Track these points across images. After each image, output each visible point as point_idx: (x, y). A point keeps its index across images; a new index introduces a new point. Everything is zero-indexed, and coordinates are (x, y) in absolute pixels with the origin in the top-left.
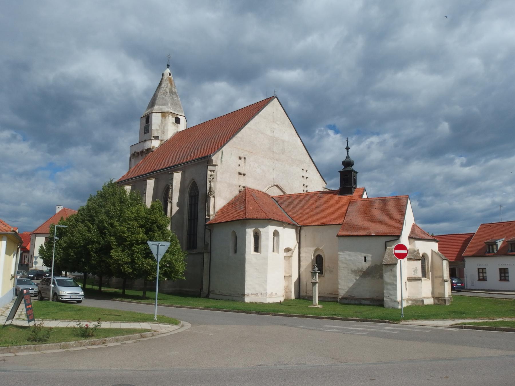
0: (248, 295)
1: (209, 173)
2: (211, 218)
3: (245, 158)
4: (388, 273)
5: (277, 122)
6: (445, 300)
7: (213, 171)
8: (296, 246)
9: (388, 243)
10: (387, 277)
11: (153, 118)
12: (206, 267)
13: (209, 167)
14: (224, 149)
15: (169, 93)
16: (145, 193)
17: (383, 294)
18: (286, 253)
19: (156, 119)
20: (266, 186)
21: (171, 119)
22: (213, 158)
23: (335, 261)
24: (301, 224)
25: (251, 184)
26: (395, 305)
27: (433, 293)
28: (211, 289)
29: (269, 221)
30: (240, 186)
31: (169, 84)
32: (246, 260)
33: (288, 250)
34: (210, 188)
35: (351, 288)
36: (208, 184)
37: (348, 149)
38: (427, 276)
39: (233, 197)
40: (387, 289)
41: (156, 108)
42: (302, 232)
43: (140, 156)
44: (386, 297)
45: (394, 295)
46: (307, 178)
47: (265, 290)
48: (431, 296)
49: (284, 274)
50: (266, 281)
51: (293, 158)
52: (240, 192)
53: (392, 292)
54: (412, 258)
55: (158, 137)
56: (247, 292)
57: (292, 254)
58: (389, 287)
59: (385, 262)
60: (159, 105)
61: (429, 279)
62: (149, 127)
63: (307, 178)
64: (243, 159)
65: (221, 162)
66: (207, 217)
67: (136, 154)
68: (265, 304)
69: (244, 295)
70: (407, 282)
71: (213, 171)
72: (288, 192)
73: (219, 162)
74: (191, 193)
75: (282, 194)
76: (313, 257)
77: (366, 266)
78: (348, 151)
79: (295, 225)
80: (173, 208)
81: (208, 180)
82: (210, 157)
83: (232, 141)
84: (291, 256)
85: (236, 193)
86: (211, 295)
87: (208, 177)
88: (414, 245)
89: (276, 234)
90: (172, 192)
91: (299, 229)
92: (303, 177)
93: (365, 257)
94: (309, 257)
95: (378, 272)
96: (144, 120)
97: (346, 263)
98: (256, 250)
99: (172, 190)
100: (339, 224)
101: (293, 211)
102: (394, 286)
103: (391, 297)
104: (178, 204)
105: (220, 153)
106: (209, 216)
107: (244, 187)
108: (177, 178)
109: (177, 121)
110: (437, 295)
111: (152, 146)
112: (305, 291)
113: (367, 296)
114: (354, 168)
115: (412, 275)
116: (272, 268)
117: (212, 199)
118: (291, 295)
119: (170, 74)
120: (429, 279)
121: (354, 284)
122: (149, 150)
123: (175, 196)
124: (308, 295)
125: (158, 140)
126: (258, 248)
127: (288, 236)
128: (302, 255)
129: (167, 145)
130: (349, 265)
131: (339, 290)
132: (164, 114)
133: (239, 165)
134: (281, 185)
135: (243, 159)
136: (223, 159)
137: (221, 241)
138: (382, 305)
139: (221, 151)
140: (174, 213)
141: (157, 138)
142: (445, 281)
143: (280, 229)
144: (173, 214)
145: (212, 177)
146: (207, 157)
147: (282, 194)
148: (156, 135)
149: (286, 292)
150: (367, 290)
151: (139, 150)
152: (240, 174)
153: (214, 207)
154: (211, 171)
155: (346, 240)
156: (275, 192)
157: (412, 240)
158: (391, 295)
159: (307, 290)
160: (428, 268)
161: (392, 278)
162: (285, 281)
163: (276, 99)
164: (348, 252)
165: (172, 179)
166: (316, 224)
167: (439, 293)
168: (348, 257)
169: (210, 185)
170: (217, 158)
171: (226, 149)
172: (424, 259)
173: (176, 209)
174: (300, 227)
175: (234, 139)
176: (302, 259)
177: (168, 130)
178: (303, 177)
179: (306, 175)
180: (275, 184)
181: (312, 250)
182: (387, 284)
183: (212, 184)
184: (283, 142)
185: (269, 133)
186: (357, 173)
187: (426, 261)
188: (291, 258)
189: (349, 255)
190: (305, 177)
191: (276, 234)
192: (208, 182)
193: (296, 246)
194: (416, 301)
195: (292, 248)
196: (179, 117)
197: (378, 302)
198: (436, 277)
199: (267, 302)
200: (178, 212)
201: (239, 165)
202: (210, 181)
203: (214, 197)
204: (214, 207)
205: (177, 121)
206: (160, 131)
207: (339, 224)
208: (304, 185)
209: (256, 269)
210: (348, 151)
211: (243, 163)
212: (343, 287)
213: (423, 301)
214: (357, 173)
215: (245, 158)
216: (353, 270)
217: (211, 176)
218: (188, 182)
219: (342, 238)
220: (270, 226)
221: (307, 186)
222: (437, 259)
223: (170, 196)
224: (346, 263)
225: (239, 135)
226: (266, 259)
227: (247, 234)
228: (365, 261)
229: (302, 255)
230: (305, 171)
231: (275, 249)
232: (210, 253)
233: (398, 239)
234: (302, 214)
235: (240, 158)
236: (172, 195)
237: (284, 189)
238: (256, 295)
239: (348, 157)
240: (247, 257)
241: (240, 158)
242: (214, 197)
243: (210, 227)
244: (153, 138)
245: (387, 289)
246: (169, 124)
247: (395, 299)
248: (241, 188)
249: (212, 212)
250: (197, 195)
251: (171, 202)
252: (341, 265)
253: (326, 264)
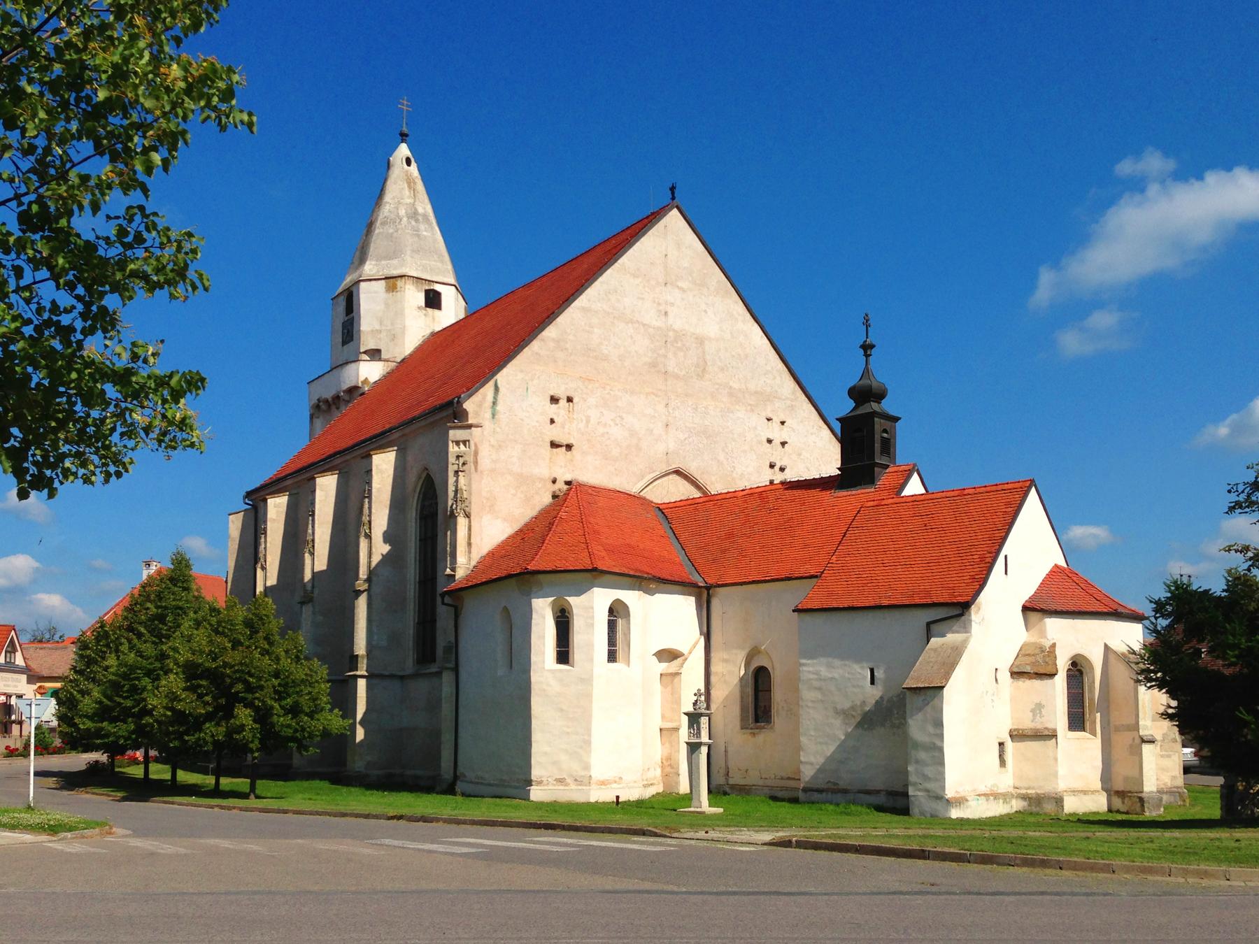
0: (540, 783)
1: (453, 449)
2: (460, 573)
3: (570, 400)
4: (920, 716)
5: (680, 284)
6: (1141, 800)
7: (464, 442)
8: (696, 643)
9: (934, 627)
10: (916, 727)
11: (362, 296)
12: (447, 709)
13: (451, 432)
14: (503, 377)
15: (405, 219)
16: (313, 515)
17: (906, 773)
18: (664, 665)
19: (371, 299)
20: (643, 477)
21: (416, 297)
22: (468, 405)
23: (794, 683)
24: (711, 581)
25: (590, 470)
26: (938, 807)
27: (1106, 777)
28: (461, 769)
29: (594, 575)
30: (554, 481)
31: (407, 192)
32: (534, 686)
33: (668, 655)
34: (456, 491)
35: (830, 759)
36: (451, 479)
37: (867, 348)
38: (1088, 725)
39: (534, 513)
40: (917, 762)
41: (369, 268)
42: (715, 603)
43: (333, 407)
44: (915, 784)
45: (937, 780)
46: (783, 444)
47: (587, 767)
48: (1098, 785)
49: (658, 723)
50: (588, 743)
51: (736, 386)
52: (555, 496)
53: (929, 771)
54: (1028, 669)
55: (379, 351)
56: (536, 773)
57: (682, 666)
58: (922, 755)
59: (910, 683)
60: (379, 259)
61: (1095, 735)
62: (352, 324)
63: (783, 444)
64: (563, 402)
65: (494, 415)
66: (448, 571)
67: (323, 407)
68: (589, 804)
69: (529, 782)
70: (1010, 746)
71: (464, 442)
72: (716, 487)
73: (488, 415)
74: (423, 508)
75: (697, 494)
76: (742, 672)
77: (873, 694)
78: (867, 356)
79: (694, 585)
80: (374, 549)
81: (452, 469)
82: (460, 403)
83: (527, 352)
84: (678, 674)
85: (547, 499)
86: (459, 787)
87: (452, 459)
88: (1043, 633)
89: (617, 612)
90: (370, 508)
91: (704, 596)
92: (770, 441)
93: (872, 671)
94: (731, 672)
95: (903, 711)
96: (342, 302)
97: (819, 689)
98: (563, 656)
99: (370, 503)
100: (812, 577)
101: (703, 544)
102: (936, 754)
103: (929, 786)
104: (387, 538)
105: (488, 390)
106: (453, 569)
107: (568, 483)
108: (384, 466)
109: (433, 300)
110: (1119, 786)
111: (362, 378)
112: (723, 771)
113: (878, 784)
114: (887, 406)
115: (1027, 724)
116: (617, 706)
117: (462, 522)
118: (677, 783)
119: (408, 162)
120: (1095, 735)
121: (842, 746)
122: (353, 390)
123: (380, 518)
124: (731, 782)
125: (380, 360)
126: (567, 652)
127: (666, 617)
128: (713, 669)
129: (406, 370)
130: (828, 694)
131: (802, 768)
132: (392, 281)
133: (552, 421)
134: (692, 468)
135: (563, 402)
136: (498, 408)
137: (477, 635)
138: (905, 811)
139: (491, 383)
140: (376, 559)
141: (375, 354)
142: (1143, 741)
143: (631, 597)
144: (374, 564)
145: (461, 460)
146: (450, 403)
147: (697, 494)
148: (372, 346)
149: (666, 776)
150: (869, 767)
151: (329, 395)
152: (554, 445)
153: (469, 544)
154: (457, 443)
155: (819, 619)
156: (674, 491)
157: (1034, 616)
158: (926, 778)
159: (727, 768)
160: (1092, 700)
161: (931, 729)
162: (663, 744)
163: (675, 211)
164: (823, 660)
165: (369, 472)
166: (751, 579)
167: (1126, 779)
168: (825, 672)
169: (457, 481)
170: (480, 405)
171: (508, 376)
172: (1081, 672)
173: (381, 549)
174: (708, 588)
175: (535, 346)
176: (713, 679)
177: (404, 329)
178: (770, 441)
179: (778, 434)
180: (674, 466)
181: (740, 656)
182: (916, 745)
183: (462, 480)
184: (701, 341)
185: (652, 318)
186: (896, 419)
187: (1086, 680)
188: (676, 680)
189: (829, 666)
190: (777, 442)
191: (617, 612)
192: (451, 474)
193: (696, 643)
194: (1035, 801)
195: (684, 649)
196: (438, 287)
197: (895, 802)
198: (1117, 729)
199: (593, 800)
200: (386, 558)
201: (552, 421)
202: (456, 472)
203: (468, 516)
204: (469, 544)
205: (433, 300)
206: (383, 335)
207: (812, 577)
208: (772, 466)
209: (562, 710)
210: (867, 356)
211: (562, 412)
212: (812, 759)
213: (1059, 801)
214: (896, 419)
215: (570, 400)
216: (839, 707)
217: (458, 457)
218: (412, 478)
219: (807, 617)
220: (597, 591)
221: (782, 469)
222: (1123, 676)
223: (365, 519)
224: (819, 689)
225: (550, 332)
226: (587, 681)
227: (534, 616)
228: (872, 682)
229: (716, 668)
230: (776, 423)
231: (620, 654)
232: (456, 670)
233: (962, 615)
234: (724, 551)
235: (554, 400)
236: (370, 516)
237: (702, 480)
238: (561, 781)
239: (866, 372)
240: (535, 677)
241: (554, 400)
242: (468, 516)
243: (458, 594)
244: (365, 357)
245: (917, 762)
246: (407, 311)
247: (940, 793)
248: (560, 485)
249: (461, 559)
250: (429, 510)
251: (368, 536)
252: (808, 695)
253: (778, 695)
